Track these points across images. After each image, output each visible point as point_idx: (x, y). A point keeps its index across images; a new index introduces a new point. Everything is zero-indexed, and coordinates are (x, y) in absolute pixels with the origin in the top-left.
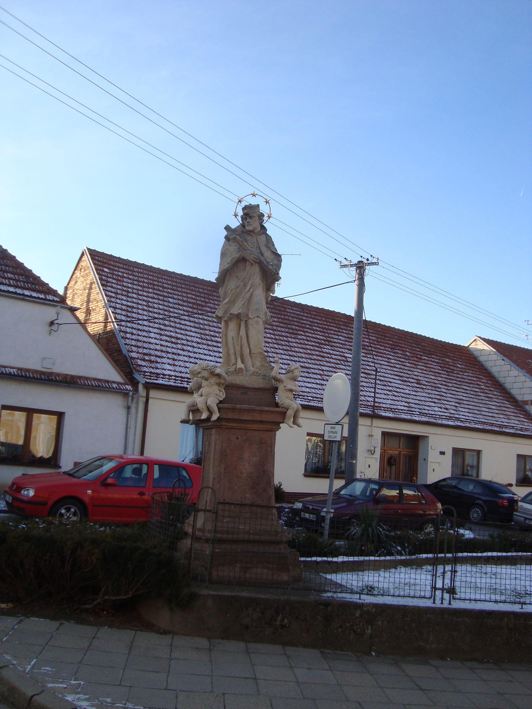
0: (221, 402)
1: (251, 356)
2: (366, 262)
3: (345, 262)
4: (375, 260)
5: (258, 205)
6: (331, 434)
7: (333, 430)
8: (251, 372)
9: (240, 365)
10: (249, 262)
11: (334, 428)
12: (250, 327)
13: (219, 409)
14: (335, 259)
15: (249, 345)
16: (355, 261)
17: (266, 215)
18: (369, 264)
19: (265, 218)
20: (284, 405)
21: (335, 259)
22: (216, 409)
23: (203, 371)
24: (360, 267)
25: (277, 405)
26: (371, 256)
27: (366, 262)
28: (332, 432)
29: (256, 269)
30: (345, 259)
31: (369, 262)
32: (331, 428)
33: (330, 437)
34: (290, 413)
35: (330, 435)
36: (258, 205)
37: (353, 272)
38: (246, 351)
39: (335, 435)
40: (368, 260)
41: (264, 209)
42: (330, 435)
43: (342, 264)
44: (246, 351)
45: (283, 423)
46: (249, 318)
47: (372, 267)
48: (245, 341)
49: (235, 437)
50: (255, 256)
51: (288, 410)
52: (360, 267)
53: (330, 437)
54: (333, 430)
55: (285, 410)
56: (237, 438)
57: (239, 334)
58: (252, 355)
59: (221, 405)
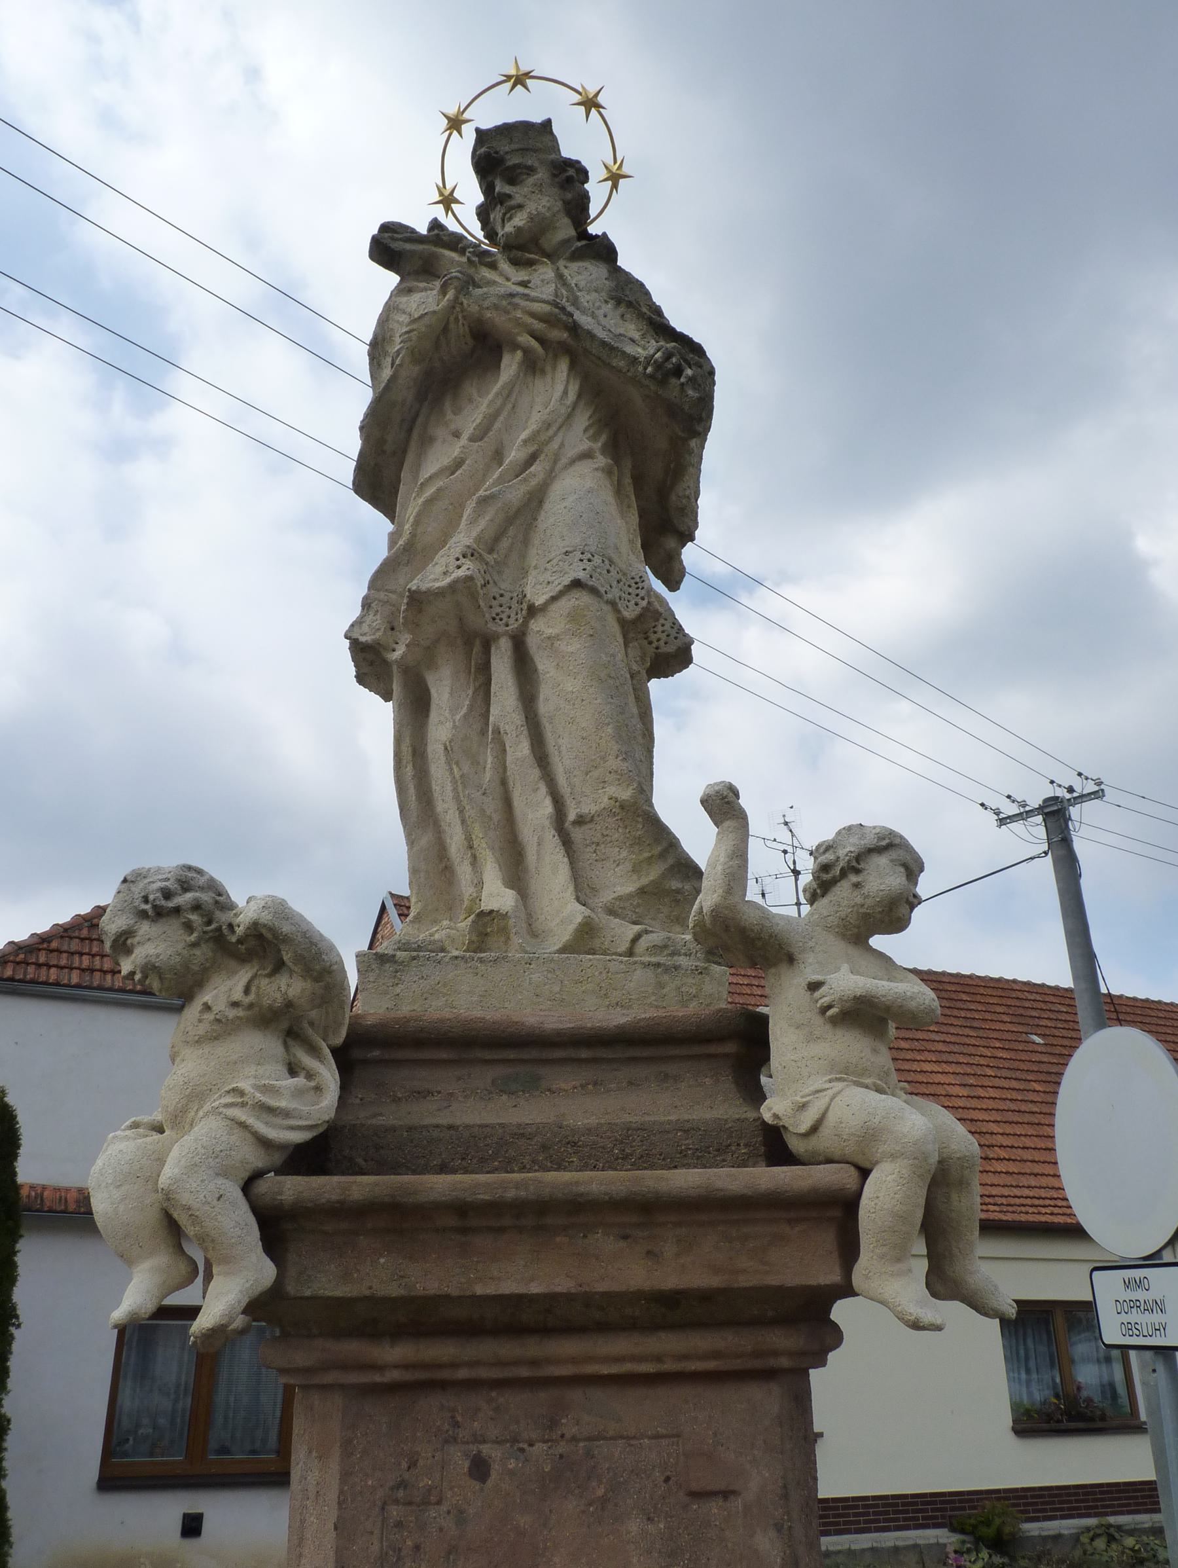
0: (312, 1156)
1: (567, 842)
2: (1068, 796)
3: (1011, 809)
4: (1091, 787)
5: (548, 123)
6: (1135, 1317)
7: (1140, 1295)
8: (565, 935)
9: (498, 896)
10: (515, 346)
11: (1139, 1284)
12: (544, 664)
13: (276, 1228)
14: (982, 805)
15: (542, 758)
16: (1035, 802)
17: (596, 173)
18: (1083, 798)
19: (597, 190)
20: (825, 1141)
21: (982, 805)
22: (237, 1223)
23: (145, 928)
24: (1055, 814)
25: (775, 1146)
26: (1080, 774)
27: (1068, 796)
28: (1135, 1305)
29: (556, 388)
30: (1009, 797)
31: (1075, 795)
32: (1127, 1284)
33: (1129, 1328)
34: (886, 1196)
35: (1125, 1318)
36: (548, 123)
37: (1037, 829)
38: (535, 812)
39: (1156, 1318)
40: (1071, 790)
41: (577, 141)
42: (1125, 1318)
43: (1002, 816)
44: (535, 812)
45: (847, 1290)
46: (532, 611)
47: (1088, 806)
48: (520, 750)
49: (459, 1461)
50: (537, 307)
51: (864, 1173)
52: (1055, 814)
53: (1129, 1328)
54: (1140, 1295)
55: (844, 1177)
56: (480, 1469)
57: (486, 715)
58: (577, 834)
59: (292, 1188)
